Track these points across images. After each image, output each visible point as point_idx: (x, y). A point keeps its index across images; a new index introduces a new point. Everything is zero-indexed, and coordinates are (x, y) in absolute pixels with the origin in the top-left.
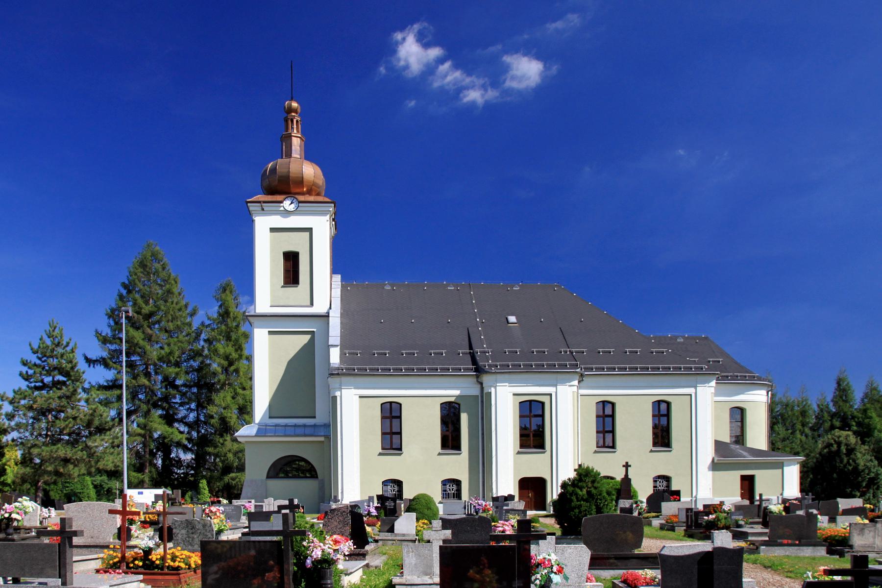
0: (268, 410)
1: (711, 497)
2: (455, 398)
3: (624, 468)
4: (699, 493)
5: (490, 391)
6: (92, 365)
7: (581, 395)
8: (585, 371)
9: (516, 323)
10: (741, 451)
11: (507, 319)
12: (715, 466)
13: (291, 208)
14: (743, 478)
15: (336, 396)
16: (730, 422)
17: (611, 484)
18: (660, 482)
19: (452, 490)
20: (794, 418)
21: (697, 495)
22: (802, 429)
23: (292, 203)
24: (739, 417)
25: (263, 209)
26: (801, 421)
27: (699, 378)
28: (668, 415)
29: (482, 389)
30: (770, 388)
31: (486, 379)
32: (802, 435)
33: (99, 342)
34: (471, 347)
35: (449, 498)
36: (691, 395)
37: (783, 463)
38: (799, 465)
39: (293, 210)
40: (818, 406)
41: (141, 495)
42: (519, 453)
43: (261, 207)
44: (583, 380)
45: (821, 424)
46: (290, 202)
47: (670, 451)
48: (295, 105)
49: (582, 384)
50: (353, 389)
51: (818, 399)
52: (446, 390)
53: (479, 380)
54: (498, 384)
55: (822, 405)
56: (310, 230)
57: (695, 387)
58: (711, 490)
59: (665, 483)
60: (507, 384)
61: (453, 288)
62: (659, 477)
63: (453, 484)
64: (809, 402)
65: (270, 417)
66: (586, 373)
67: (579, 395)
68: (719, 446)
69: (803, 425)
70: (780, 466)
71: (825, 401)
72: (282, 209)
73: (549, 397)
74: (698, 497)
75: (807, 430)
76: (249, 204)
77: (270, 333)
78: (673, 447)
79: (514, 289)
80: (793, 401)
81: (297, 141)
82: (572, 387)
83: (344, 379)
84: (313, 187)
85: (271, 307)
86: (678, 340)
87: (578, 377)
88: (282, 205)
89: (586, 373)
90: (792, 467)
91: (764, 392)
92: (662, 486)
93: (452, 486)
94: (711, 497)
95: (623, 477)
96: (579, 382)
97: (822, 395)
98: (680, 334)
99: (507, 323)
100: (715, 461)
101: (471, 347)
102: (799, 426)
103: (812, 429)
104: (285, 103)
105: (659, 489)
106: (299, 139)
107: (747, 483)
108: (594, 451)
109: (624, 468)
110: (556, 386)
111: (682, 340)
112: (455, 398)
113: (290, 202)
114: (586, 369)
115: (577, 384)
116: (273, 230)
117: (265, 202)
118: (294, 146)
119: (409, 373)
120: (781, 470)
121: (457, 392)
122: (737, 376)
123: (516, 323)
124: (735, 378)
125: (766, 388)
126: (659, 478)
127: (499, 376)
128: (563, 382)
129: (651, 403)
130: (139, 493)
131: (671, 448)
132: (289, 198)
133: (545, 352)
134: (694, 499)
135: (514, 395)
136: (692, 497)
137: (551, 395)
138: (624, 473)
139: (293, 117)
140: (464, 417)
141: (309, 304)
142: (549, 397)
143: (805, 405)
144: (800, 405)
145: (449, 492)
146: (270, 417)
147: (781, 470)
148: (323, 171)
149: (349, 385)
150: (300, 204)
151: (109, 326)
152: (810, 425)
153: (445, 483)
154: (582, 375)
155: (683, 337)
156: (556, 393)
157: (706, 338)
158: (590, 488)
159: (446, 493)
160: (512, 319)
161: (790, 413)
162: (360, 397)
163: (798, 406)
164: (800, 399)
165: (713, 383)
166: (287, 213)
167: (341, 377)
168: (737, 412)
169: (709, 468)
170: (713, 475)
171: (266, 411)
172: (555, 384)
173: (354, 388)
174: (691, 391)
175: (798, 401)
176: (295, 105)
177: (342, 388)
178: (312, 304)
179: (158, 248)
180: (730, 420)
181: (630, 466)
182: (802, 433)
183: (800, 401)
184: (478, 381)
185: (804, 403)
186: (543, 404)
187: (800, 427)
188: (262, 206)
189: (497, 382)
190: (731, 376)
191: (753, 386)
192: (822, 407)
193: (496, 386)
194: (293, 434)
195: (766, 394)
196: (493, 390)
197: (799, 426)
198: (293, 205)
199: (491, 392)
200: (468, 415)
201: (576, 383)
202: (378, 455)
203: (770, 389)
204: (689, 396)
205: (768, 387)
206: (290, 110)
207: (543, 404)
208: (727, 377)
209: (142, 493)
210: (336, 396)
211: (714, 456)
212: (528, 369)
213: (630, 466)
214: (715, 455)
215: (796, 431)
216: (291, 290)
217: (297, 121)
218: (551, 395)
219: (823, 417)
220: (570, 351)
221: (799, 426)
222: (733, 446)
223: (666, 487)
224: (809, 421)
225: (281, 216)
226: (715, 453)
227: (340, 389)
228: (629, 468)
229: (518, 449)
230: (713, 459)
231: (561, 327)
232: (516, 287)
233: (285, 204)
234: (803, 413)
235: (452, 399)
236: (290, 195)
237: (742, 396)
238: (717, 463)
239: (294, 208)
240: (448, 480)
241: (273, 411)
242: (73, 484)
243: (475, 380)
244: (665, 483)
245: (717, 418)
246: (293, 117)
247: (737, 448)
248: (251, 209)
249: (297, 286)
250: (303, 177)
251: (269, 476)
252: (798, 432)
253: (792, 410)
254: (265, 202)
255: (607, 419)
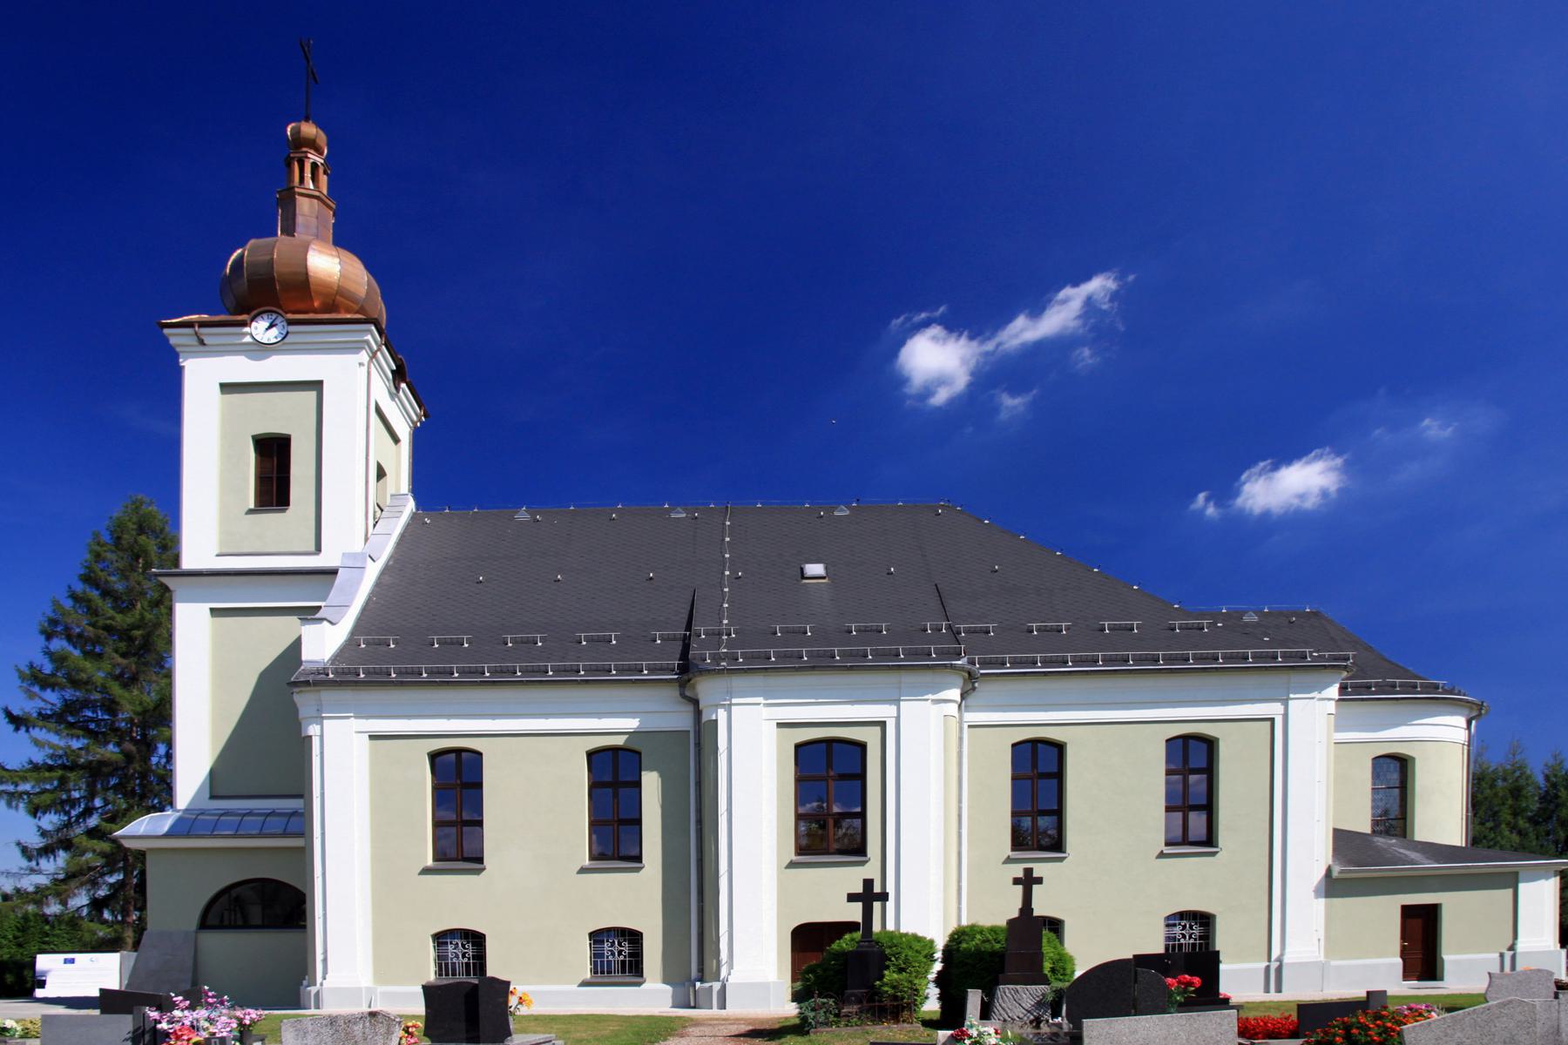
0: (208, 781)
1: (1322, 958)
2: (626, 736)
3: (1020, 888)
4: (1288, 949)
5: (714, 718)
6: (23, 729)
7: (969, 726)
8: (980, 668)
9: (824, 578)
10: (1402, 851)
11: (802, 570)
12: (1333, 887)
13: (272, 336)
14: (1407, 911)
15: (311, 737)
16: (1373, 789)
17: (978, 936)
18: (1184, 927)
19: (620, 953)
20: (1496, 801)
21: (1282, 954)
22: (1512, 821)
23: (271, 326)
24: (1395, 777)
25: (202, 343)
26: (1511, 807)
27: (1296, 678)
28: (1210, 770)
29: (698, 713)
30: (1476, 712)
31: (706, 688)
32: (1511, 832)
33: (23, 682)
34: (689, 627)
35: (1168, 926)
36: (1272, 720)
37: (1516, 874)
38: (1558, 878)
39: (275, 341)
40: (1547, 778)
41: (69, 965)
42: (792, 865)
43: (196, 338)
44: (974, 689)
45: (1553, 811)
46: (267, 324)
47: (1214, 854)
48: (309, 129)
49: (971, 700)
50: (352, 719)
51: (1546, 765)
52: (600, 718)
53: (688, 693)
54: (734, 701)
55: (1555, 776)
56: (317, 386)
57: (1285, 702)
58: (1322, 942)
59: (1197, 930)
60: (760, 700)
61: (684, 515)
62: (1182, 915)
63: (621, 939)
64: (1528, 772)
65: (213, 797)
66: (982, 671)
67: (966, 725)
68: (1343, 841)
69: (1515, 815)
70: (1511, 881)
71: (1562, 768)
72: (248, 339)
73: (878, 729)
74: (1286, 960)
75: (1522, 823)
76: (166, 331)
77: (215, 612)
78: (1220, 844)
79: (836, 513)
80: (1493, 771)
81: (312, 206)
82: (943, 705)
83: (327, 695)
84: (338, 297)
85: (218, 555)
86: (1246, 619)
87: (960, 682)
88: (247, 329)
89: (982, 671)
90: (1542, 882)
91: (1461, 721)
92: (1190, 937)
93: (620, 944)
94: (1322, 958)
95: (1016, 914)
96: (963, 696)
97: (1555, 757)
98: (1252, 607)
99: (799, 578)
100: (1335, 874)
101: (689, 627)
102: (1506, 815)
103: (1533, 821)
104: (286, 131)
105: (1181, 945)
106: (316, 201)
107: (1417, 923)
108: (1006, 856)
109: (1020, 888)
110: (897, 702)
111: (1256, 619)
112: (626, 736)
113: (267, 324)
114: (984, 664)
115: (959, 699)
116: (226, 388)
117: (203, 324)
118: (303, 215)
119: (502, 679)
120: (1510, 891)
121: (632, 724)
122: (1394, 686)
123: (824, 578)
124: (1381, 689)
125: (1466, 712)
126: (1182, 919)
127: (738, 681)
128: (918, 692)
129: (1164, 742)
130: (66, 961)
131: (1217, 847)
132: (265, 316)
133: (881, 631)
134: (1274, 965)
135: (780, 725)
136: (1269, 960)
137: (882, 725)
138: (1019, 904)
139: (303, 155)
140: (651, 784)
141: (312, 548)
142: (878, 729)
143: (1519, 777)
144: (1508, 777)
145: (610, 958)
146: (213, 797)
147: (1510, 891)
148: (370, 267)
149: (342, 710)
150: (292, 328)
151: (46, 653)
152: (1529, 814)
153: (597, 937)
154: (971, 677)
155: (1259, 612)
156: (898, 718)
157: (1316, 614)
158: (245, 1014)
159: (602, 962)
160: (814, 569)
161: (1488, 792)
162: (372, 737)
163: (1505, 780)
164: (1509, 767)
165: (1333, 691)
166: (260, 350)
167: (319, 691)
168: (1392, 766)
169: (1317, 893)
170: (1327, 907)
171: (204, 783)
172: (896, 698)
173: (356, 717)
174: (1273, 709)
175: (1505, 771)
176: (309, 129)
177: (323, 718)
178: (318, 549)
179: (153, 508)
180: (1374, 784)
181: (1039, 881)
182: (1513, 828)
183: (1507, 770)
184: (683, 695)
185: (1518, 774)
186: (862, 747)
187: (1509, 818)
188: (196, 333)
189: (731, 694)
190: (1377, 685)
191: (1433, 707)
192: (1554, 780)
193: (731, 705)
194: (280, 831)
195: (1465, 726)
196: (722, 715)
197: (1506, 815)
198: (274, 331)
199: (716, 721)
200: (661, 776)
201: (955, 694)
202: (421, 873)
203: (1474, 714)
204: (1268, 724)
205: (1471, 709)
206: (301, 143)
207: (862, 747)
208: (1368, 687)
209: (72, 961)
210: (311, 737)
211: (1330, 862)
212: (822, 664)
213: (1039, 881)
214: (1334, 861)
215: (1500, 824)
216: (271, 519)
217: (315, 166)
218: (882, 725)
219: (1557, 797)
220: (949, 627)
221: (1505, 816)
222: (1380, 841)
223: (1201, 938)
224: (1528, 806)
225: (247, 357)
226: (1335, 850)
227: (319, 720)
228: (1035, 888)
229: (791, 855)
230: (1329, 871)
231: (936, 582)
232: (842, 510)
233: (256, 328)
234: (1516, 792)
235: (619, 741)
236: (275, 309)
237: (1404, 728)
238: (1337, 879)
239: (276, 337)
240: (609, 930)
241: (217, 783)
242: (55, 945)
243: (674, 692)
244: (1197, 930)
245: (1340, 780)
246: (303, 155)
247: (1393, 845)
248: (173, 341)
249: (284, 511)
250: (307, 274)
251: (204, 925)
252: (1503, 826)
253: (1492, 786)
254: (203, 324)
255: (1042, 783)
